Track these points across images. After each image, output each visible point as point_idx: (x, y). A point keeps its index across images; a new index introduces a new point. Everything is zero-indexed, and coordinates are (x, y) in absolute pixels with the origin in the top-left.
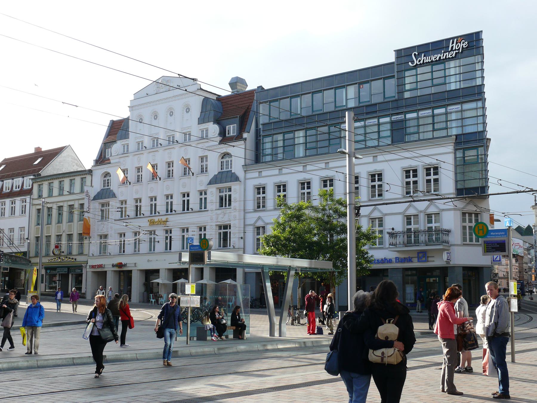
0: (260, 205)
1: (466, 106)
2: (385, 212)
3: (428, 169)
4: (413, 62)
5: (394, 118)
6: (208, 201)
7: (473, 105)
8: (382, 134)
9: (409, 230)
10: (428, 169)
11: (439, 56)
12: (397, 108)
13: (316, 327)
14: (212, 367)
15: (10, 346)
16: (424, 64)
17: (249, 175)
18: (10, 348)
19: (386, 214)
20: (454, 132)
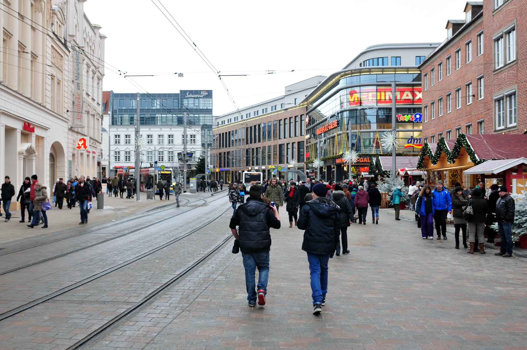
0: (117, 142)
1: (206, 115)
2: (121, 150)
3: (191, 136)
4: (187, 96)
5: (179, 115)
6: (103, 139)
7: (209, 115)
8: (174, 121)
9: (148, 156)
10: (191, 136)
11: (197, 96)
12: (180, 112)
13: (56, 183)
14: (495, 268)
15: (20, 219)
16: (191, 98)
17: (111, 130)
18: (20, 222)
19: (121, 150)
20: (201, 124)
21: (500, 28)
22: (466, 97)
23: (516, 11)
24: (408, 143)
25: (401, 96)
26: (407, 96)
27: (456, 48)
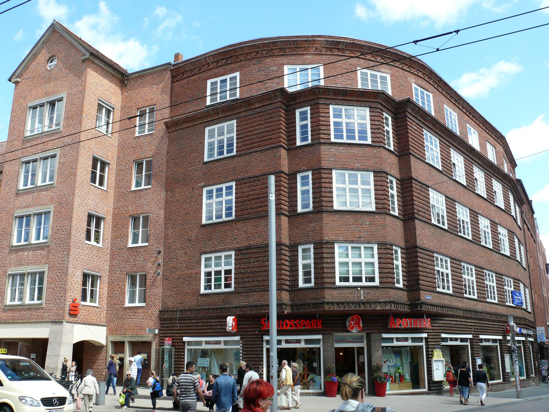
23: (53, 199)
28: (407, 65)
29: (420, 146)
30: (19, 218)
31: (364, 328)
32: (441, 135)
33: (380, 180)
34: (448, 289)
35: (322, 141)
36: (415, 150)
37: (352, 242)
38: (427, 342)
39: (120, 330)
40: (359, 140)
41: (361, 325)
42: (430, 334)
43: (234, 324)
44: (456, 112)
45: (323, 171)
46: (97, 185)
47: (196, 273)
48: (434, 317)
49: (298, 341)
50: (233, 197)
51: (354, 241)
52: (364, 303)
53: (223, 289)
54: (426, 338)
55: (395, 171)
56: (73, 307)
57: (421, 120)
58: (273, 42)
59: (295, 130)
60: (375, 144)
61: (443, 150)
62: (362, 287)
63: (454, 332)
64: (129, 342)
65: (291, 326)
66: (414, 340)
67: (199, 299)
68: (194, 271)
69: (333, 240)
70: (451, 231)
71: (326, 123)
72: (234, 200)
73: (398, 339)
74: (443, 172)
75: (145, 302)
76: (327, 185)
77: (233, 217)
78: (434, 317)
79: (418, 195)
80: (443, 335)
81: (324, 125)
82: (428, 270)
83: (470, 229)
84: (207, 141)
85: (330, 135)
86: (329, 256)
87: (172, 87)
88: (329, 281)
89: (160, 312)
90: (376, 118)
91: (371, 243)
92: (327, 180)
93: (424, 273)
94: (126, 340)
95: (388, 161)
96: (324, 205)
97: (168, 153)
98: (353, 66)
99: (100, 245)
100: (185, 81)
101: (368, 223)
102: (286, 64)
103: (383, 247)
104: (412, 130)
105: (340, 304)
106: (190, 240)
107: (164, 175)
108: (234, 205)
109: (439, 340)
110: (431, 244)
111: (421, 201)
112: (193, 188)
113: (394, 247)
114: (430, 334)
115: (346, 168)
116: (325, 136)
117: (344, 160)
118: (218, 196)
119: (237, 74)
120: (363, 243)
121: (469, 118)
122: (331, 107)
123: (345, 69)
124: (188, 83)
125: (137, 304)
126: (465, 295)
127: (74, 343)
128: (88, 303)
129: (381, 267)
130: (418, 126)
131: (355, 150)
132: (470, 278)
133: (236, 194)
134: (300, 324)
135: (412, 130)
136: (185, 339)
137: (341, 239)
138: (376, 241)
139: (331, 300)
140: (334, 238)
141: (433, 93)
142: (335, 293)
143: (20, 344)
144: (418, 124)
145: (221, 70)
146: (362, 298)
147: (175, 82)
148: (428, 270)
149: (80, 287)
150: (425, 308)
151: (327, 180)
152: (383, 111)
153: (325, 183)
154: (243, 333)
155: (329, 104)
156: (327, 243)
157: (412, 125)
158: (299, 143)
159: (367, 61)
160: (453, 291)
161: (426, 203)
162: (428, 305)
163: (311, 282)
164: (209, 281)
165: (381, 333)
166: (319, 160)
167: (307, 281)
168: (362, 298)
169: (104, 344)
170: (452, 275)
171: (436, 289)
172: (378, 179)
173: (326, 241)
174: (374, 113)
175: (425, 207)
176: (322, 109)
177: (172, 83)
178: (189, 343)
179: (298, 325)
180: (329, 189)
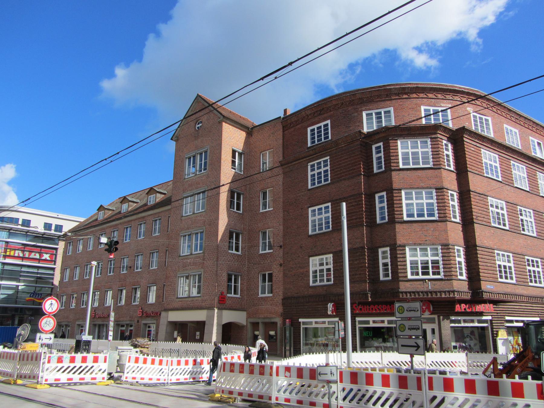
21: (188, 229)
22: (120, 268)
23: (205, 222)
24: (30, 297)
25: (29, 255)
26: (35, 255)
27: (112, 228)
28: (465, 97)
29: (478, 163)
30: (184, 236)
31: (435, 312)
32: (500, 151)
33: (441, 195)
34: (511, 278)
35: (393, 168)
36: (473, 168)
37: (420, 244)
38: (491, 323)
39: (256, 314)
40: (423, 164)
41: (432, 309)
42: (493, 317)
43: (333, 309)
44: (517, 129)
45: (394, 191)
46: (235, 210)
47: (307, 271)
48: (495, 302)
49: (383, 322)
50: (330, 214)
51: (422, 244)
52: (431, 292)
53: (325, 283)
54: (491, 321)
55: (455, 186)
56: (222, 298)
57: (479, 142)
58: (353, 94)
59: (372, 161)
60: (436, 167)
61: (502, 163)
62: (430, 280)
63: (518, 315)
64: (262, 323)
65: (376, 310)
66: (480, 321)
67: (309, 290)
68: (305, 270)
69: (405, 244)
70: (513, 230)
71: (395, 154)
72: (330, 217)
73: (465, 321)
74: (503, 182)
75: (272, 293)
76: (398, 202)
77: (331, 229)
78: (495, 302)
79: (476, 203)
80: (507, 318)
81: (393, 156)
82: (489, 264)
83: (534, 227)
84: (310, 173)
85: (398, 163)
86: (401, 256)
87: (283, 135)
88: (402, 276)
89: (282, 300)
90: (436, 145)
91: (436, 245)
92: (398, 198)
93: (485, 267)
94: (260, 321)
95: (448, 179)
96: (396, 217)
97: (283, 184)
98: (418, 106)
99: (240, 253)
100: (292, 129)
101: (432, 229)
102: (364, 110)
103: (445, 248)
104: (470, 151)
105: (412, 293)
106: (301, 247)
107: (281, 200)
108: (330, 220)
109: (503, 322)
110: (491, 242)
111: (480, 208)
112: (302, 209)
113: (456, 247)
114: (493, 317)
115: (413, 187)
116: (395, 165)
117: (411, 181)
118: (319, 214)
119: (328, 122)
120: (428, 245)
121: (532, 132)
122: (399, 142)
123: (411, 108)
124: (294, 131)
125: (267, 295)
126: (530, 284)
127: (223, 324)
128: (233, 295)
129: (445, 263)
130: (475, 147)
131: (419, 173)
132: (536, 269)
133: (332, 211)
134: (382, 308)
135: (470, 151)
136: (301, 320)
137: (411, 242)
138: (439, 243)
139: (404, 290)
140: (405, 242)
141: (491, 116)
142: (408, 284)
143: (189, 325)
144: (476, 146)
145: (316, 119)
146: (430, 288)
147: (285, 131)
148: (489, 264)
149: (226, 284)
150: (485, 296)
151: (398, 198)
152: (443, 139)
153: (396, 200)
154: (341, 316)
155: (397, 140)
156: (400, 246)
157: (469, 148)
158: (375, 171)
159: (429, 99)
160: (516, 281)
161: (485, 209)
162: (486, 292)
163: (331, 281)
164: (315, 277)
165: (449, 316)
166: (391, 183)
167: (387, 275)
168: (430, 288)
169: (245, 324)
170: (514, 267)
171: (498, 280)
172: (439, 195)
173: (398, 245)
174: (434, 142)
175: (485, 213)
176: (392, 144)
177: (283, 132)
178: (304, 323)
179: (381, 309)
180: (400, 205)
